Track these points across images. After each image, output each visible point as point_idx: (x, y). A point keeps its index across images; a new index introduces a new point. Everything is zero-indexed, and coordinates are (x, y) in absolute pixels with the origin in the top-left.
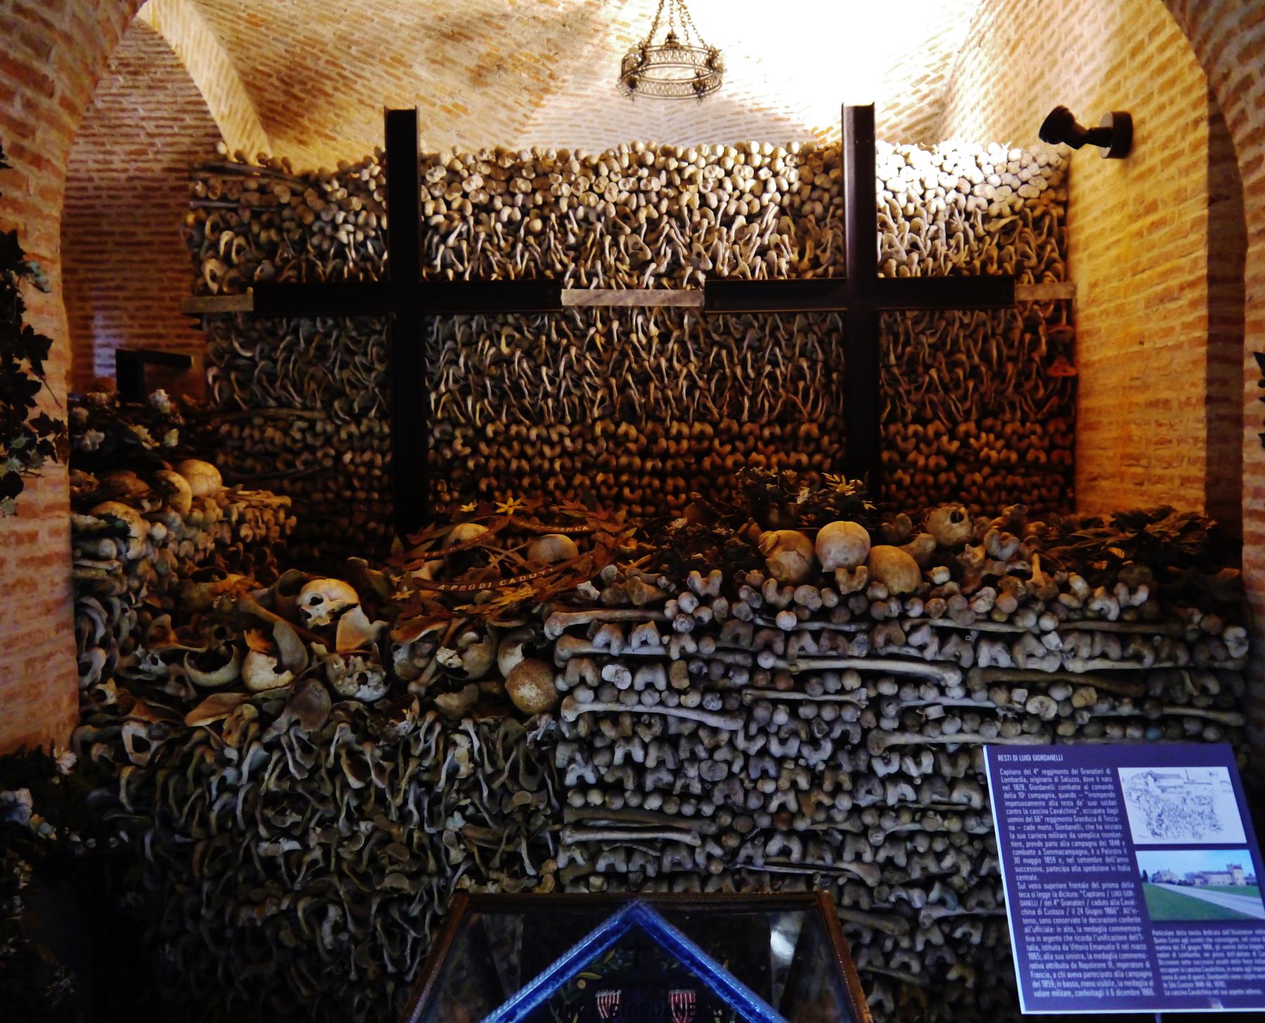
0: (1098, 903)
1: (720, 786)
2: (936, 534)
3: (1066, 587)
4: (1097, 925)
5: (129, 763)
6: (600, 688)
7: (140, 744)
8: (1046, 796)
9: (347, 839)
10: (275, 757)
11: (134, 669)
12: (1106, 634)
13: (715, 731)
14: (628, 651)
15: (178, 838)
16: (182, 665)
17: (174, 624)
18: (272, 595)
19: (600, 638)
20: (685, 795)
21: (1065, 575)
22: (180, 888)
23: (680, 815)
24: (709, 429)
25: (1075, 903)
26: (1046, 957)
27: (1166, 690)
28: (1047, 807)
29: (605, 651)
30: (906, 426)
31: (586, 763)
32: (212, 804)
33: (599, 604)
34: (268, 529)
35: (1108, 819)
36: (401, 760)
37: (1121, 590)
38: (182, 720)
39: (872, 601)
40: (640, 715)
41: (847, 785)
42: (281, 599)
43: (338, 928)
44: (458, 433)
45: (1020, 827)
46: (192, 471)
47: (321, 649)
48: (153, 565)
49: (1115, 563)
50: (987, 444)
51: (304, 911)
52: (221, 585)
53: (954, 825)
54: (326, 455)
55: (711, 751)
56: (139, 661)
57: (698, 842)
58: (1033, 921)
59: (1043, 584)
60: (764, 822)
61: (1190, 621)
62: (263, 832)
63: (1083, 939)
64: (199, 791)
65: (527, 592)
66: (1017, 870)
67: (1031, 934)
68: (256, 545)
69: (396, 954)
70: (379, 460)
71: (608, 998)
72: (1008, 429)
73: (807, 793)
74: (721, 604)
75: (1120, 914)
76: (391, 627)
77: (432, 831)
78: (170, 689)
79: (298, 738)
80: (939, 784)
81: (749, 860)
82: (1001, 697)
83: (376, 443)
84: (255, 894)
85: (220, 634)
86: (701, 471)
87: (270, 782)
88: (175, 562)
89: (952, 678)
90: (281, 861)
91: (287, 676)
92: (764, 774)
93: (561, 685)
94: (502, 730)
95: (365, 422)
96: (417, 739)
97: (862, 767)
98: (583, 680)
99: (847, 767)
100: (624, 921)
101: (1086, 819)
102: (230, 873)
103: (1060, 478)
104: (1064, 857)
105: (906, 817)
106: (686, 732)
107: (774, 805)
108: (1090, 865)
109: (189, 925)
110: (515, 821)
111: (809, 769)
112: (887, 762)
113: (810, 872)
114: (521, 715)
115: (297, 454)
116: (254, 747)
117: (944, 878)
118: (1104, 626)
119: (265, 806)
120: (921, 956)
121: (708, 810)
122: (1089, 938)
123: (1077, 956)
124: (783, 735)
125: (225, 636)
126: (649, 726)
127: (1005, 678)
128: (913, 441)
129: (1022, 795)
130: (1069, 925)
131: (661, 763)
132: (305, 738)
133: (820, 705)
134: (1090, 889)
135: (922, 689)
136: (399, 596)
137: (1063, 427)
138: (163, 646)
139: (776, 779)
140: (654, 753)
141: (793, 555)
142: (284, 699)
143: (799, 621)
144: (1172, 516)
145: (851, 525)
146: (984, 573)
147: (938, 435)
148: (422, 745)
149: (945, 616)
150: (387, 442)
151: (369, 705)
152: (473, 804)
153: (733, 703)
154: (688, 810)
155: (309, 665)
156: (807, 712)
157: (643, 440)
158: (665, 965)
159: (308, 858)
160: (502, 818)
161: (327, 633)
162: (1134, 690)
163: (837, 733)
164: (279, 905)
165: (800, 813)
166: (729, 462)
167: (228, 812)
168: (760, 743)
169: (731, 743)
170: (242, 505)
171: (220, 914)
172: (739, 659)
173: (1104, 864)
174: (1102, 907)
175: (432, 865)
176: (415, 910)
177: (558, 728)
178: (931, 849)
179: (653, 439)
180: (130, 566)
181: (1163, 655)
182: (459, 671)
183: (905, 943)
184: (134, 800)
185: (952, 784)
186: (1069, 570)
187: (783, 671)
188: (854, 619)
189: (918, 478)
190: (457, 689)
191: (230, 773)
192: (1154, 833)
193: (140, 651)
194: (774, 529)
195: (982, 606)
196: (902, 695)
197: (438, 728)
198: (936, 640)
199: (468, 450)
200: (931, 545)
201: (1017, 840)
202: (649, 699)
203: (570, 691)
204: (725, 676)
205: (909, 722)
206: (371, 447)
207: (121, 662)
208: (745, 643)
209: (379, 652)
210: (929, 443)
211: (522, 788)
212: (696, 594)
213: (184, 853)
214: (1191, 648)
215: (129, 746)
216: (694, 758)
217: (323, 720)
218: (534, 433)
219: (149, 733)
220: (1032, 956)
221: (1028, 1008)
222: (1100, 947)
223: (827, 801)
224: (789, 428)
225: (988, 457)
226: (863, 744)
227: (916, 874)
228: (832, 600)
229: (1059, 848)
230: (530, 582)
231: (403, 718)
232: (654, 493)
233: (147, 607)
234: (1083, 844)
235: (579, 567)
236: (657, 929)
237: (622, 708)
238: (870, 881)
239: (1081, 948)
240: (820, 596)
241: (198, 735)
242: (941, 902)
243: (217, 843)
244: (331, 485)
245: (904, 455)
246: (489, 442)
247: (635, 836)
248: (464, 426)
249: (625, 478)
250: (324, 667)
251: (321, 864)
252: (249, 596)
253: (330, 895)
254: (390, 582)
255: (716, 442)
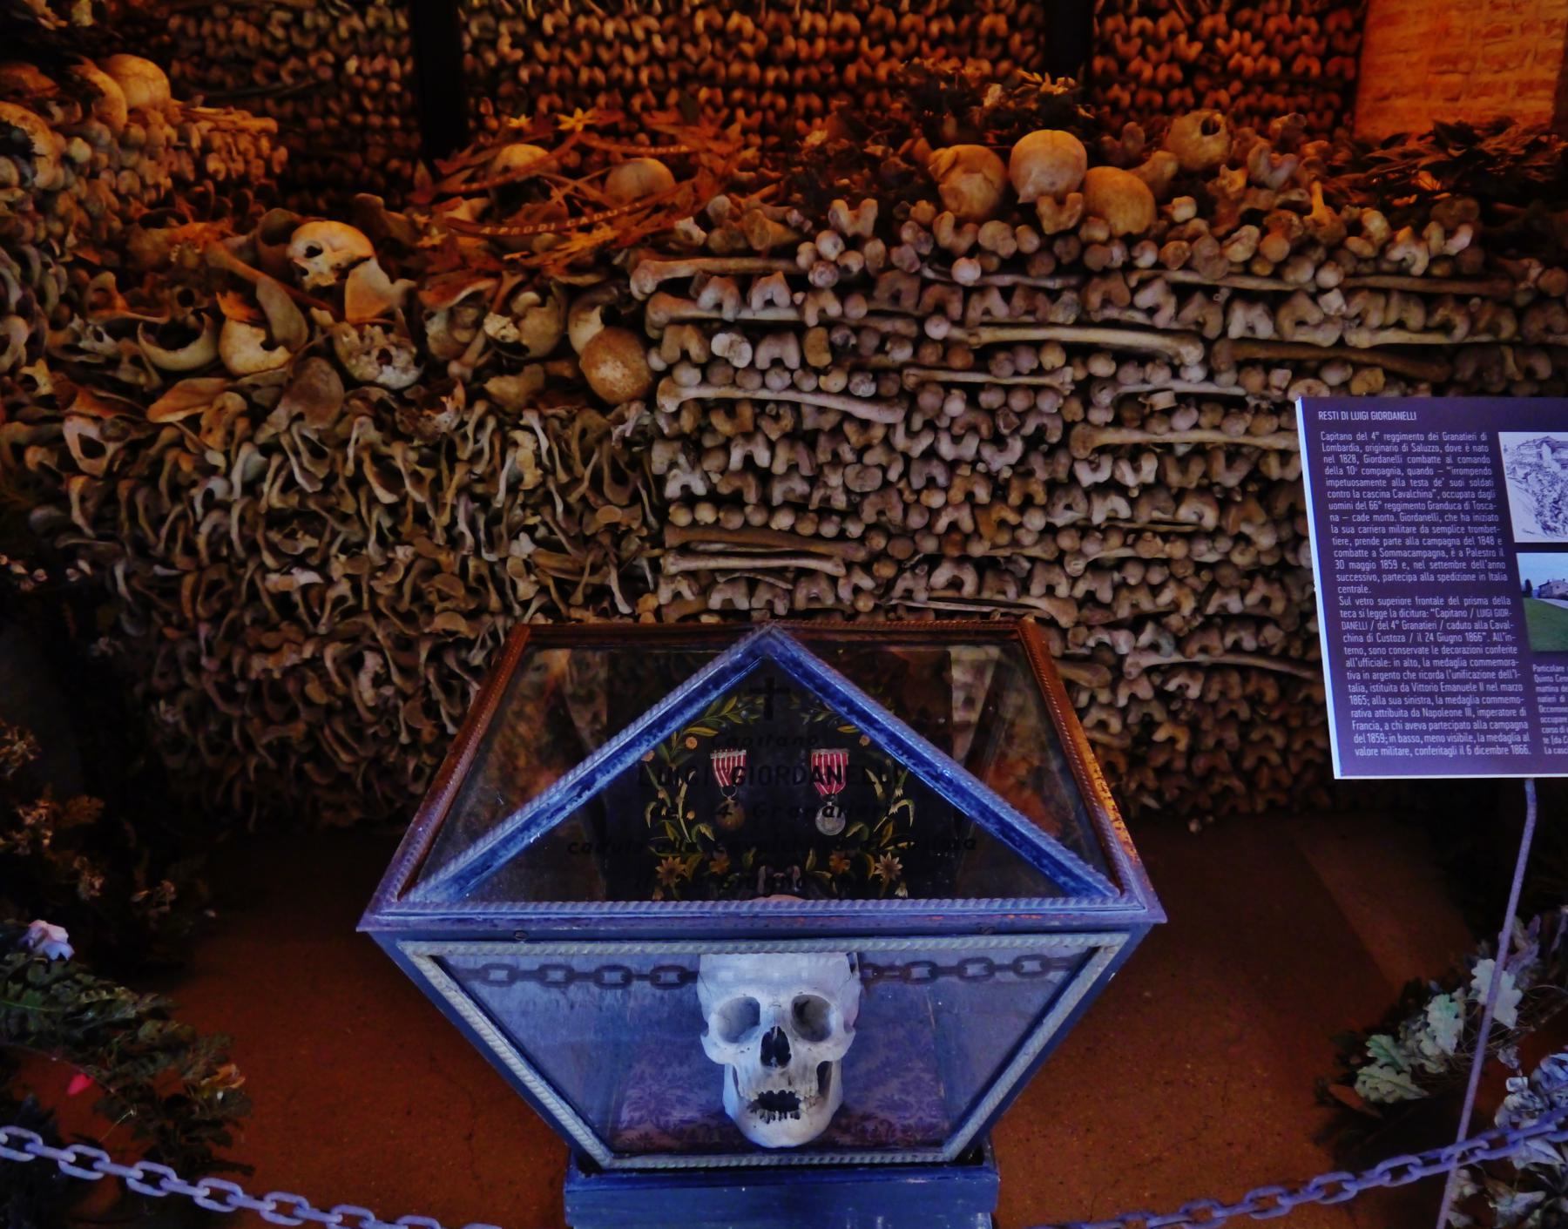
0: (1457, 626)
1: (872, 498)
2: (1178, 152)
3: (1356, 228)
4: (1453, 657)
5: (80, 473)
6: (708, 366)
7: (91, 448)
8: (1388, 472)
9: (381, 568)
10: (276, 461)
11: (73, 349)
12: (1406, 294)
13: (865, 424)
14: (746, 315)
15: (158, 570)
16: (136, 340)
17: (122, 285)
18: (252, 245)
19: (708, 297)
20: (825, 511)
21: (1356, 211)
22: (170, 633)
23: (817, 537)
24: (854, 23)
25: (1422, 626)
26: (1375, 701)
27: (1478, 374)
28: (1389, 488)
29: (714, 315)
30: (1128, 20)
31: (693, 468)
32: (198, 525)
33: (704, 251)
34: (247, 162)
35: (1480, 506)
36: (444, 465)
37: (1434, 232)
38: (143, 414)
39: (1086, 245)
40: (762, 404)
41: (1041, 498)
42: (264, 249)
43: (378, 681)
44: (503, 28)
45: (1346, 518)
46: (124, 71)
47: (324, 316)
48: (80, 203)
49: (1426, 197)
50: (1240, 48)
51: (334, 660)
52: (181, 231)
53: (1177, 550)
54: (322, 62)
55: (860, 453)
56: (77, 337)
57: (841, 571)
58: (1360, 651)
59: (1327, 220)
60: (930, 545)
61: (1524, 277)
62: (269, 560)
63: (1431, 676)
64: (178, 509)
65: (604, 233)
66: (1340, 578)
67: (1356, 670)
68: (233, 185)
69: (457, 712)
70: (396, 69)
71: (727, 761)
72: (1272, 25)
73: (985, 508)
74: (876, 248)
75: (1487, 642)
76: (421, 287)
77: (492, 557)
78: (125, 374)
79: (304, 439)
80: (1162, 497)
81: (909, 594)
82: (1255, 379)
83: (389, 44)
84: (269, 639)
85: (186, 299)
86: (842, 87)
87: (272, 495)
88: (113, 199)
89: (1191, 353)
90: (297, 597)
91: (280, 355)
92: (931, 483)
93: (657, 363)
94: (578, 425)
95: (372, 11)
96: (465, 437)
97: (1062, 475)
98: (685, 355)
99: (1041, 474)
100: (751, 654)
101: (1446, 506)
102: (232, 614)
103: (1335, 99)
104: (1410, 561)
105: (1115, 540)
106: (827, 427)
107: (942, 524)
108: (1449, 572)
109: (189, 678)
110: (601, 545)
111: (991, 477)
112: (1095, 468)
113: (986, 609)
114: (603, 405)
115: (281, 60)
116: (246, 450)
117: (1158, 618)
118: (1404, 283)
119: (269, 527)
120: (1123, 712)
121: (854, 530)
122: (1440, 676)
123: (1421, 700)
124: (957, 430)
125: (192, 305)
126: (777, 418)
127: (1262, 354)
128: (1138, 42)
129: (1352, 470)
130: (1413, 657)
131: (793, 468)
132: (314, 437)
133: (1008, 389)
134: (1445, 607)
135: (1149, 368)
136: (426, 242)
137: (1348, 23)
138: (106, 313)
139: (946, 490)
140: (783, 454)
141: (978, 178)
142: (280, 386)
143: (984, 273)
144: (1512, 130)
145: (1060, 135)
146: (1244, 207)
147: (1173, 33)
148: (470, 446)
149: (1187, 266)
150: (406, 44)
151: (398, 393)
152: (545, 523)
153: (890, 387)
154: (829, 530)
155: (310, 338)
156: (989, 399)
157: (763, 38)
158: (807, 718)
159: (332, 594)
160: (585, 542)
161: (333, 296)
162: (1437, 372)
163: (1030, 428)
164: (300, 652)
165: (977, 533)
166: (882, 72)
167: (219, 537)
168: (925, 441)
169: (887, 442)
170: (205, 126)
171: (226, 664)
172: (900, 326)
173: (1469, 571)
174: (1461, 632)
175: (494, 601)
176: (477, 658)
177: (654, 421)
178: (1144, 581)
179: (776, 38)
180: (45, 200)
181: (1482, 324)
182: (518, 348)
183: (1104, 697)
184: (95, 521)
185: (1179, 497)
186: (1362, 205)
187: (959, 343)
188: (1059, 270)
189: (1142, 96)
190: (514, 370)
191: (217, 485)
192: (1546, 527)
193: (76, 323)
194: (947, 145)
195: (1239, 252)
196: (1122, 376)
197: (491, 423)
198: (1173, 301)
199: (519, 54)
200: (1170, 168)
201: (1340, 536)
202: (777, 380)
203: (669, 371)
204: (880, 349)
205: (1127, 414)
206: (384, 50)
207: (52, 339)
208: (908, 304)
209: (408, 322)
210: (1159, 47)
211: (609, 502)
212: (841, 234)
213: (169, 589)
214: (1520, 315)
215: (76, 451)
216: (837, 462)
217: (335, 412)
218: (609, 29)
219: (102, 431)
220: (1355, 700)
221: (1343, 772)
222: (1455, 688)
223: (1012, 518)
224: (966, 21)
225: (1240, 67)
226: (1064, 444)
227: (1124, 612)
228: (1030, 242)
229: (1403, 547)
230: (609, 221)
231: (443, 408)
232: (779, 116)
233: (79, 262)
234: (1439, 542)
235: (678, 199)
236: (797, 664)
237: (739, 394)
238: (1064, 621)
239: (1428, 688)
240: (1015, 236)
241: (166, 435)
242: (1154, 647)
243: (212, 575)
244: (333, 105)
245: (1123, 62)
246: (548, 41)
247: (759, 563)
248: (512, 18)
249: (737, 95)
250: (330, 341)
251: (351, 602)
252: (219, 245)
253: (367, 641)
254: (413, 223)
255: (865, 43)
